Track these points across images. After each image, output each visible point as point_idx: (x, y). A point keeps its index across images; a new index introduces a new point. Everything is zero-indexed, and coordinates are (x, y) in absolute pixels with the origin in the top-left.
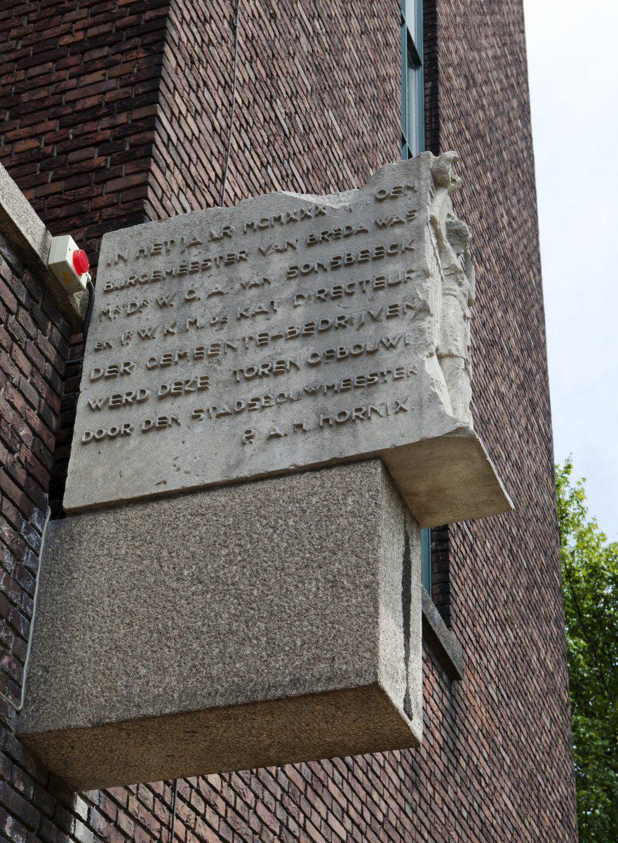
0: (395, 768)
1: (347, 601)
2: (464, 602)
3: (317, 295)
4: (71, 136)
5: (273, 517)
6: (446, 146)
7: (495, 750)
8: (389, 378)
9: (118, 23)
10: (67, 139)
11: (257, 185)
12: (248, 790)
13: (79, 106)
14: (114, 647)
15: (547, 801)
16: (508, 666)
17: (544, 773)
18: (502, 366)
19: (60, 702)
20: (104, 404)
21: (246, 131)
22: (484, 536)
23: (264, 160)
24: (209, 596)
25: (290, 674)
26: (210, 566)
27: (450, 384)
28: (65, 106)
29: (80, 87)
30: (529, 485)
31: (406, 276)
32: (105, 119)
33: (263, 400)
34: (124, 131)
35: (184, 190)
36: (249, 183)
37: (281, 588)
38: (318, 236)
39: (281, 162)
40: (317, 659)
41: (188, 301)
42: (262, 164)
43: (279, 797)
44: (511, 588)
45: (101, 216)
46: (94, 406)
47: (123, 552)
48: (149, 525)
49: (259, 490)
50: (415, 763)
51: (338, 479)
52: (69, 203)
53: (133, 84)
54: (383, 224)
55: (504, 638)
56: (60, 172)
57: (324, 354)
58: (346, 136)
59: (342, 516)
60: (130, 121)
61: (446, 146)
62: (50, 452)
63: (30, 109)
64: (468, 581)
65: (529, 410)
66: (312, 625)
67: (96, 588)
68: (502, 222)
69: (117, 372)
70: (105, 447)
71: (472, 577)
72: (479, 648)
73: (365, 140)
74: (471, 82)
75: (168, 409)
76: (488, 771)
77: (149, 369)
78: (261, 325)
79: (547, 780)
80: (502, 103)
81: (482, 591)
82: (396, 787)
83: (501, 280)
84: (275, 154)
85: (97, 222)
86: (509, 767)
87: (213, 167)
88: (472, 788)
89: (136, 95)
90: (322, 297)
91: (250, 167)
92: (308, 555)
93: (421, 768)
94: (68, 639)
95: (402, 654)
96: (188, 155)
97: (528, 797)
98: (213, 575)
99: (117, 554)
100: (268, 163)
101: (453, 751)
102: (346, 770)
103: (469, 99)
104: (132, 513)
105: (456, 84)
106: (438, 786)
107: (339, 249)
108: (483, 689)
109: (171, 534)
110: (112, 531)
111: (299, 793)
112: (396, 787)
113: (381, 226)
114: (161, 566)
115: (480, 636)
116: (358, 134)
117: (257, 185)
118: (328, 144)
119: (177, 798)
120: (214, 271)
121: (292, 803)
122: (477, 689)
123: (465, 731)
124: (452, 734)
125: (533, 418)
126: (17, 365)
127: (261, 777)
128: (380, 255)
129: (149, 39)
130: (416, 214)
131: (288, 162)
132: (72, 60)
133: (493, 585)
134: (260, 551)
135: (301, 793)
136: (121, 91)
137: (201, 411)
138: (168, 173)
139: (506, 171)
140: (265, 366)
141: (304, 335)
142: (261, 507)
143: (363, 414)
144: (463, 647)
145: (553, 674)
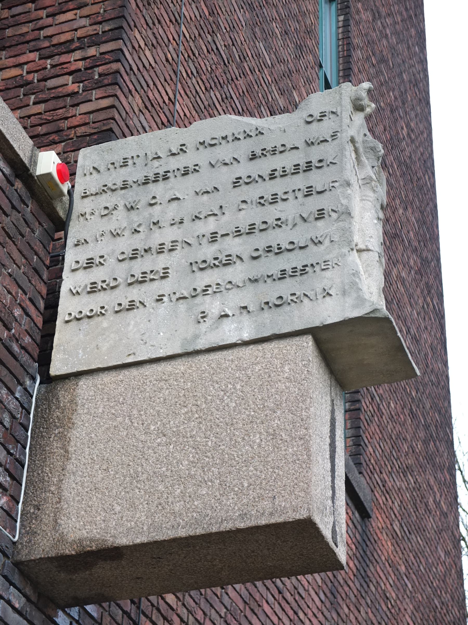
0: (317, 591)
1: (285, 450)
2: (372, 453)
3: (258, 201)
4: (49, 66)
5: (224, 382)
6: (356, 70)
7: (399, 577)
8: (317, 268)
10: (46, 68)
11: (202, 107)
12: (198, 609)
13: (55, 40)
14: (93, 488)
15: (442, 621)
16: (409, 506)
17: (440, 597)
18: (403, 255)
19: (49, 534)
20: (83, 289)
21: (193, 61)
22: (389, 398)
23: (208, 85)
24: (171, 447)
25: (239, 509)
26: (172, 422)
27: (367, 274)
28: (43, 40)
29: (56, 25)
30: (426, 355)
31: (331, 185)
32: (77, 52)
33: (215, 287)
34: (94, 63)
35: (144, 112)
36: (195, 105)
37: (231, 439)
38: (258, 152)
39: (221, 87)
40: (261, 497)
41: (151, 205)
42: (206, 89)
43: (223, 615)
44: (411, 441)
45: (75, 133)
46: (74, 291)
47: (100, 410)
48: (121, 389)
49: (212, 360)
50: (333, 588)
51: (276, 351)
52: (49, 122)
53: (100, 23)
54: (312, 142)
55: (406, 483)
56: (40, 96)
57: (264, 249)
58: (274, 64)
59: (280, 381)
60: (98, 55)
61: (356, 70)
62: (39, 329)
63: (14, 43)
64: (376, 435)
65: (426, 292)
66: (256, 470)
67: (78, 440)
68: (403, 134)
69: (92, 263)
70: (85, 323)
71: (379, 432)
72: (385, 492)
73: (289, 66)
74: (377, 15)
75: (135, 293)
76: (394, 595)
77: (120, 261)
78: (211, 225)
79: (443, 603)
80: (402, 32)
81: (387, 443)
82: (318, 608)
83: (401, 183)
84: (216, 80)
85: (72, 139)
86: (410, 592)
87: (166, 91)
88: (380, 610)
89: (103, 32)
91: (196, 91)
92: (253, 413)
93: (338, 592)
94: (55, 482)
95: (330, 493)
96: (146, 82)
97: (427, 618)
98: (175, 429)
99: (95, 413)
100: (211, 88)
101: (364, 577)
102: (277, 592)
103: (374, 30)
104: (106, 378)
105: (364, 17)
106: (352, 608)
107: (277, 162)
108: (389, 526)
109: (140, 396)
110: (91, 394)
111: (240, 612)
112: (318, 608)
113: (309, 144)
114: (132, 423)
115: (385, 481)
116: (281, 61)
117: (202, 107)
118: (259, 71)
119: (141, 615)
120: (172, 179)
121: (233, 620)
122: (384, 526)
123: (374, 561)
124: (364, 565)
125: (428, 299)
126: (11, 257)
127: (208, 598)
128: (309, 167)
130: (338, 134)
131: (227, 87)
133: (396, 439)
134: (213, 410)
135: (242, 612)
136: (90, 28)
137: (163, 295)
138: (130, 97)
139: (406, 90)
140: (216, 259)
141: (248, 233)
142: (213, 374)
143: (297, 298)
144: (372, 491)
145: (446, 514)
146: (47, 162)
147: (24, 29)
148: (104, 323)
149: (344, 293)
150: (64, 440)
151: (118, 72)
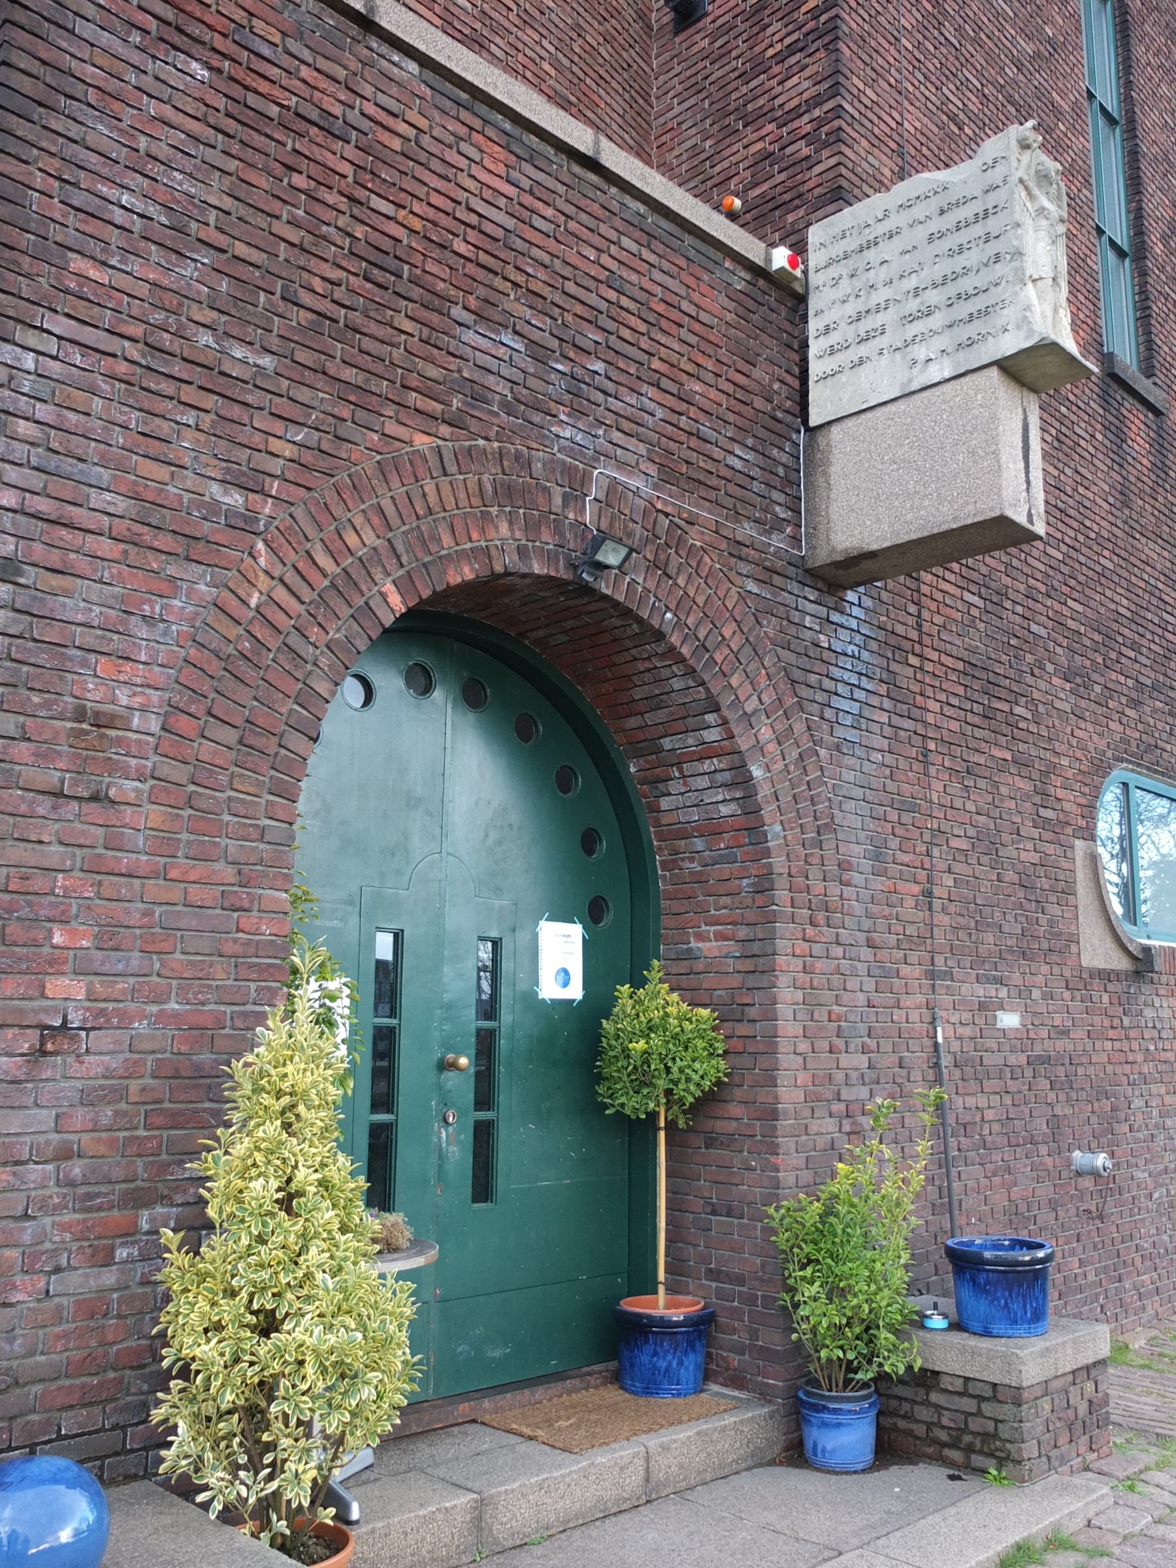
9: (804, 30)
13: (787, 108)
34: (819, 123)
52: (791, 188)
75: (863, 350)
90: (951, 253)
104: (850, 423)
129: (827, 39)
132: (776, 69)
146: (780, 257)
147: (761, 102)
148: (843, 378)
149: (1018, 327)
150: (825, 474)
151: (840, 128)
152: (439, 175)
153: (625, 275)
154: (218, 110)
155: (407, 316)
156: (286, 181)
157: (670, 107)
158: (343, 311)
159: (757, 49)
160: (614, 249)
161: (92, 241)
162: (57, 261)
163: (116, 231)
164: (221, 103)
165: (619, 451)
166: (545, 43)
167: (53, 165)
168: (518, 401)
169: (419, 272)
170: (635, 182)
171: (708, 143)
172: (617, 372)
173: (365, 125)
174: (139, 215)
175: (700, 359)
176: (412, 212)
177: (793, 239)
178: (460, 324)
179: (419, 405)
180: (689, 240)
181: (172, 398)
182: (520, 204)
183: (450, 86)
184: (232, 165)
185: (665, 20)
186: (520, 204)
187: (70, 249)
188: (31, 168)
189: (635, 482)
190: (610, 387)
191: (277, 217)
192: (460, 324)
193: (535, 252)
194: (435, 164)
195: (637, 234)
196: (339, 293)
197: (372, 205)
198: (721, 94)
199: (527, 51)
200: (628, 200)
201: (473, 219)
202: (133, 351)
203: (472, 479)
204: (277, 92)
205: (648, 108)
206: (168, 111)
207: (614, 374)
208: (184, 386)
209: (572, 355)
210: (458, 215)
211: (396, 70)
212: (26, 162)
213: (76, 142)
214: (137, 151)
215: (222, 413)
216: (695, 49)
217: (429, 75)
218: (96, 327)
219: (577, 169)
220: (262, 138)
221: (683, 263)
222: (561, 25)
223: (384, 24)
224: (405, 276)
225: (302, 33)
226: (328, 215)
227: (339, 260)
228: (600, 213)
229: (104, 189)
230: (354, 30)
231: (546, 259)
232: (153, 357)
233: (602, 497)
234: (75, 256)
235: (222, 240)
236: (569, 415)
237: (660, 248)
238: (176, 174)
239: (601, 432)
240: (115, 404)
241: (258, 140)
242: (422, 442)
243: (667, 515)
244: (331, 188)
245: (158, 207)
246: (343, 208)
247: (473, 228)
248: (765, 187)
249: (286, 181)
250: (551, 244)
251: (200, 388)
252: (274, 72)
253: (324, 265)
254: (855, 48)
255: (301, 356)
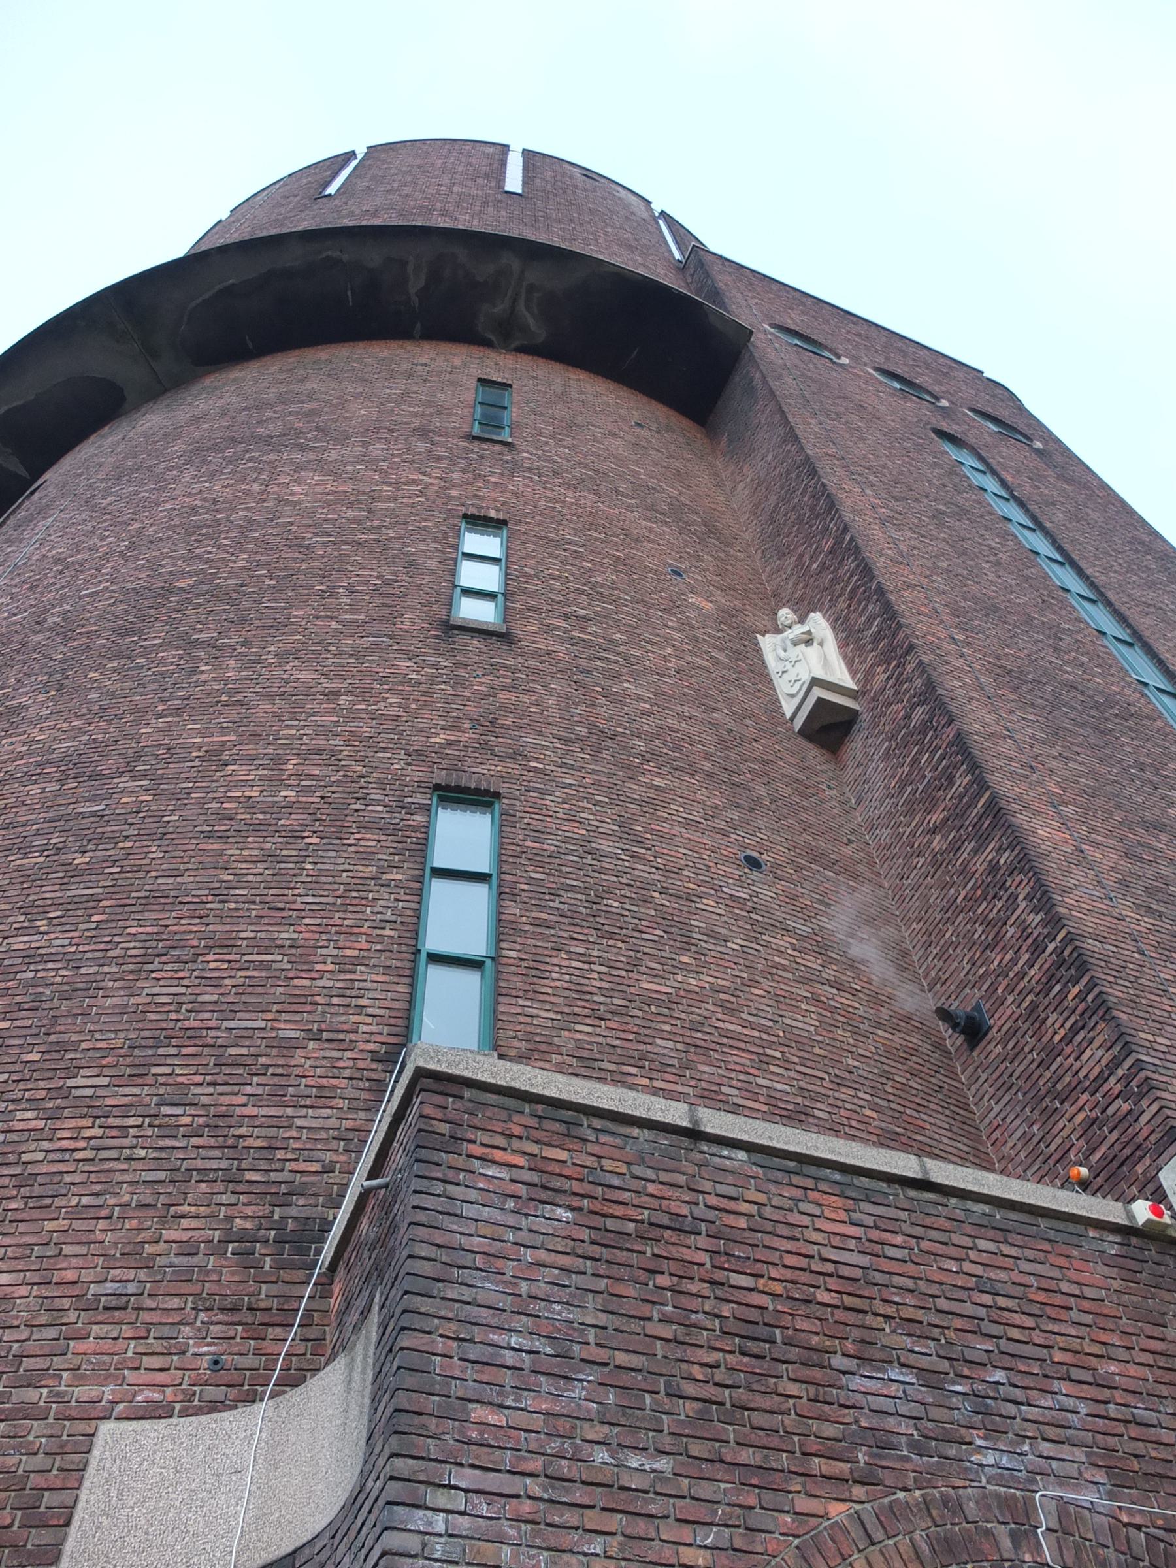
9: (1078, 1011)
34: (1127, 1080)
129: (1101, 1012)
132: (1068, 1050)
146: (1142, 1211)
147: (1067, 1079)
151: (1147, 1078)
152: (787, 1238)
153: (992, 1275)
154: (583, 1241)
155: (790, 1379)
156: (651, 1283)
157: (989, 1109)
158: (727, 1392)
159: (1045, 1040)
160: (973, 1255)
161: (488, 1387)
162: (459, 1416)
163: (509, 1372)
164: (585, 1234)
165: (1054, 1464)
166: (861, 1095)
167: (451, 1328)
168: (927, 1437)
169: (790, 1332)
170: (970, 1187)
171: (1035, 1128)
172: (1020, 1376)
173: (711, 1215)
174: (526, 1351)
175: (1104, 1337)
176: (770, 1278)
177: (1151, 1187)
178: (844, 1373)
179: (825, 1470)
180: (1043, 1223)
181: (577, 1528)
182: (869, 1241)
183: (778, 1160)
184: (602, 1284)
185: (959, 1042)
186: (869, 1241)
187: (470, 1401)
188: (433, 1336)
189: (1087, 1497)
190: (1018, 1394)
191: (649, 1319)
192: (844, 1373)
193: (898, 1280)
194: (782, 1230)
195: (991, 1233)
196: (720, 1375)
197: (733, 1283)
198: (1029, 1084)
199: (848, 1106)
200: (970, 1205)
201: (829, 1268)
202: (534, 1487)
203: (904, 1541)
204: (631, 1211)
205: (971, 1116)
206: (542, 1255)
207: (1017, 1380)
208: (587, 1512)
209: (966, 1372)
210: (813, 1268)
211: (727, 1162)
212: (429, 1333)
213: (469, 1303)
214: (520, 1295)
215: (628, 1531)
216: (992, 1057)
217: (757, 1157)
218: (499, 1471)
219: (912, 1193)
220: (625, 1253)
221: (1046, 1246)
222: (870, 1076)
223: (708, 1130)
224: (779, 1339)
225: (643, 1158)
226: (695, 1304)
227: (713, 1343)
228: (947, 1225)
229: (494, 1338)
230: (686, 1142)
231: (909, 1283)
232: (553, 1488)
233: (1054, 1525)
234: (475, 1405)
235: (602, 1355)
236: (985, 1438)
237: (1018, 1240)
238: (554, 1306)
239: (1026, 1448)
240: (523, 1548)
241: (621, 1256)
242: (837, 1511)
243: (1138, 1527)
244: (692, 1278)
245: (543, 1340)
246: (706, 1293)
247: (831, 1275)
248: (1103, 1149)
249: (651, 1283)
250: (910, 1268)
251: (604, 1509)
252: (626, 1196)
253: (700, 1352)
254: (1130, 1011)
255: (696, 1449)
